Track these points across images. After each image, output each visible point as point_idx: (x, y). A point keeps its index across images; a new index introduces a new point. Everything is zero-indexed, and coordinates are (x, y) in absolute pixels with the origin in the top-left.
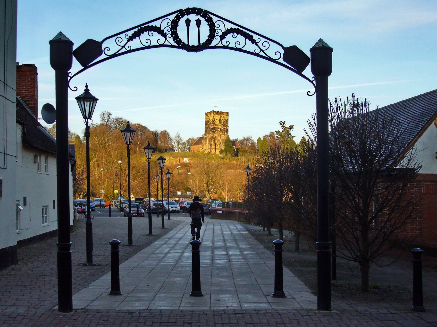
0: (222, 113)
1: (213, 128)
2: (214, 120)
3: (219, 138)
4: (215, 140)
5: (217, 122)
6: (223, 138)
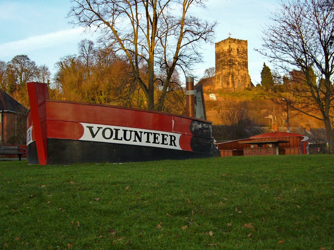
0: (239, 41)
1: (230, 61)
2: (230, 51)
3: (237, 74)
4: (233, 76)
5: (234, 53)
6: (242, 74)
